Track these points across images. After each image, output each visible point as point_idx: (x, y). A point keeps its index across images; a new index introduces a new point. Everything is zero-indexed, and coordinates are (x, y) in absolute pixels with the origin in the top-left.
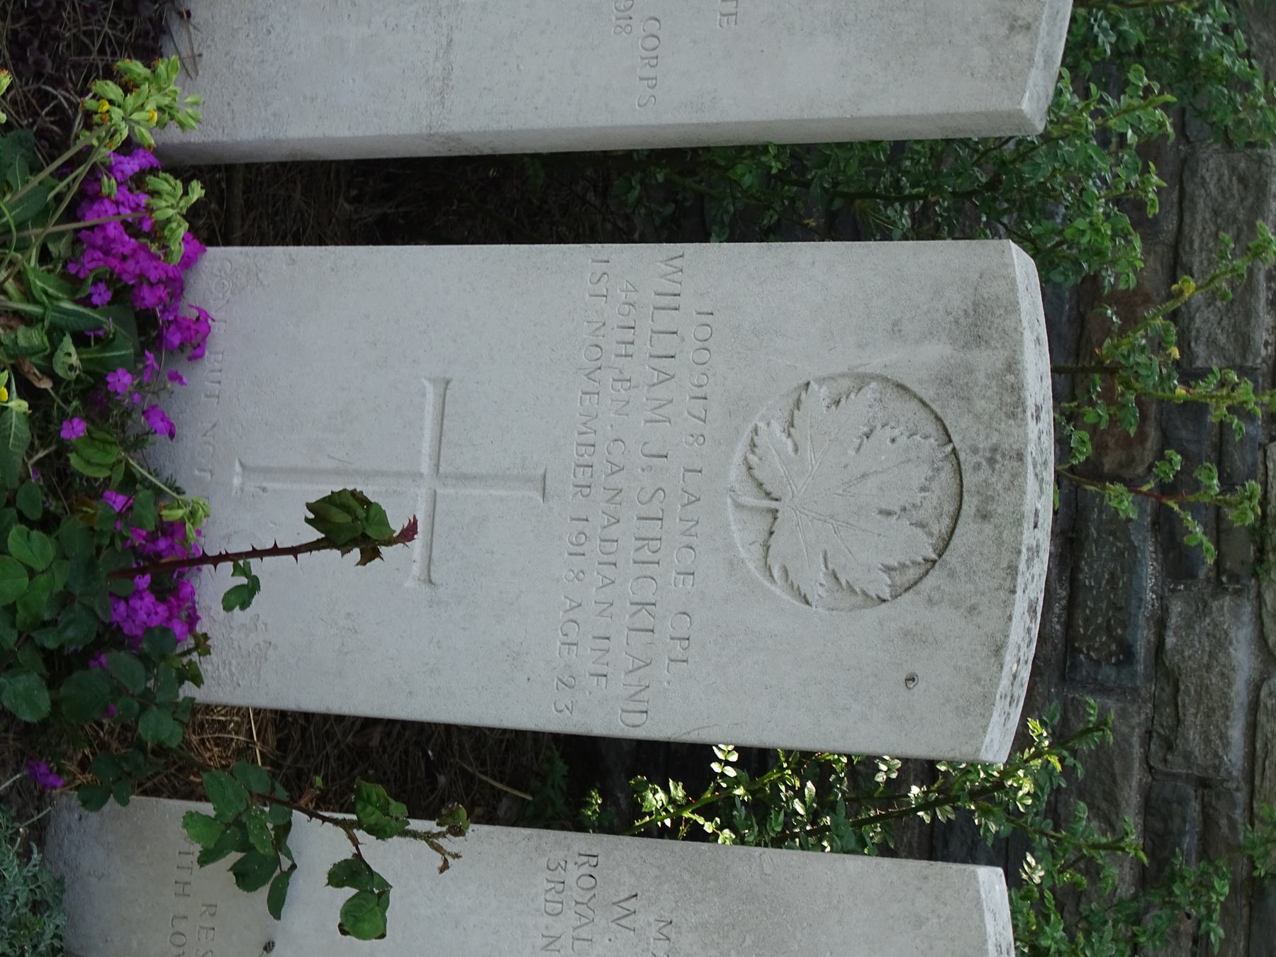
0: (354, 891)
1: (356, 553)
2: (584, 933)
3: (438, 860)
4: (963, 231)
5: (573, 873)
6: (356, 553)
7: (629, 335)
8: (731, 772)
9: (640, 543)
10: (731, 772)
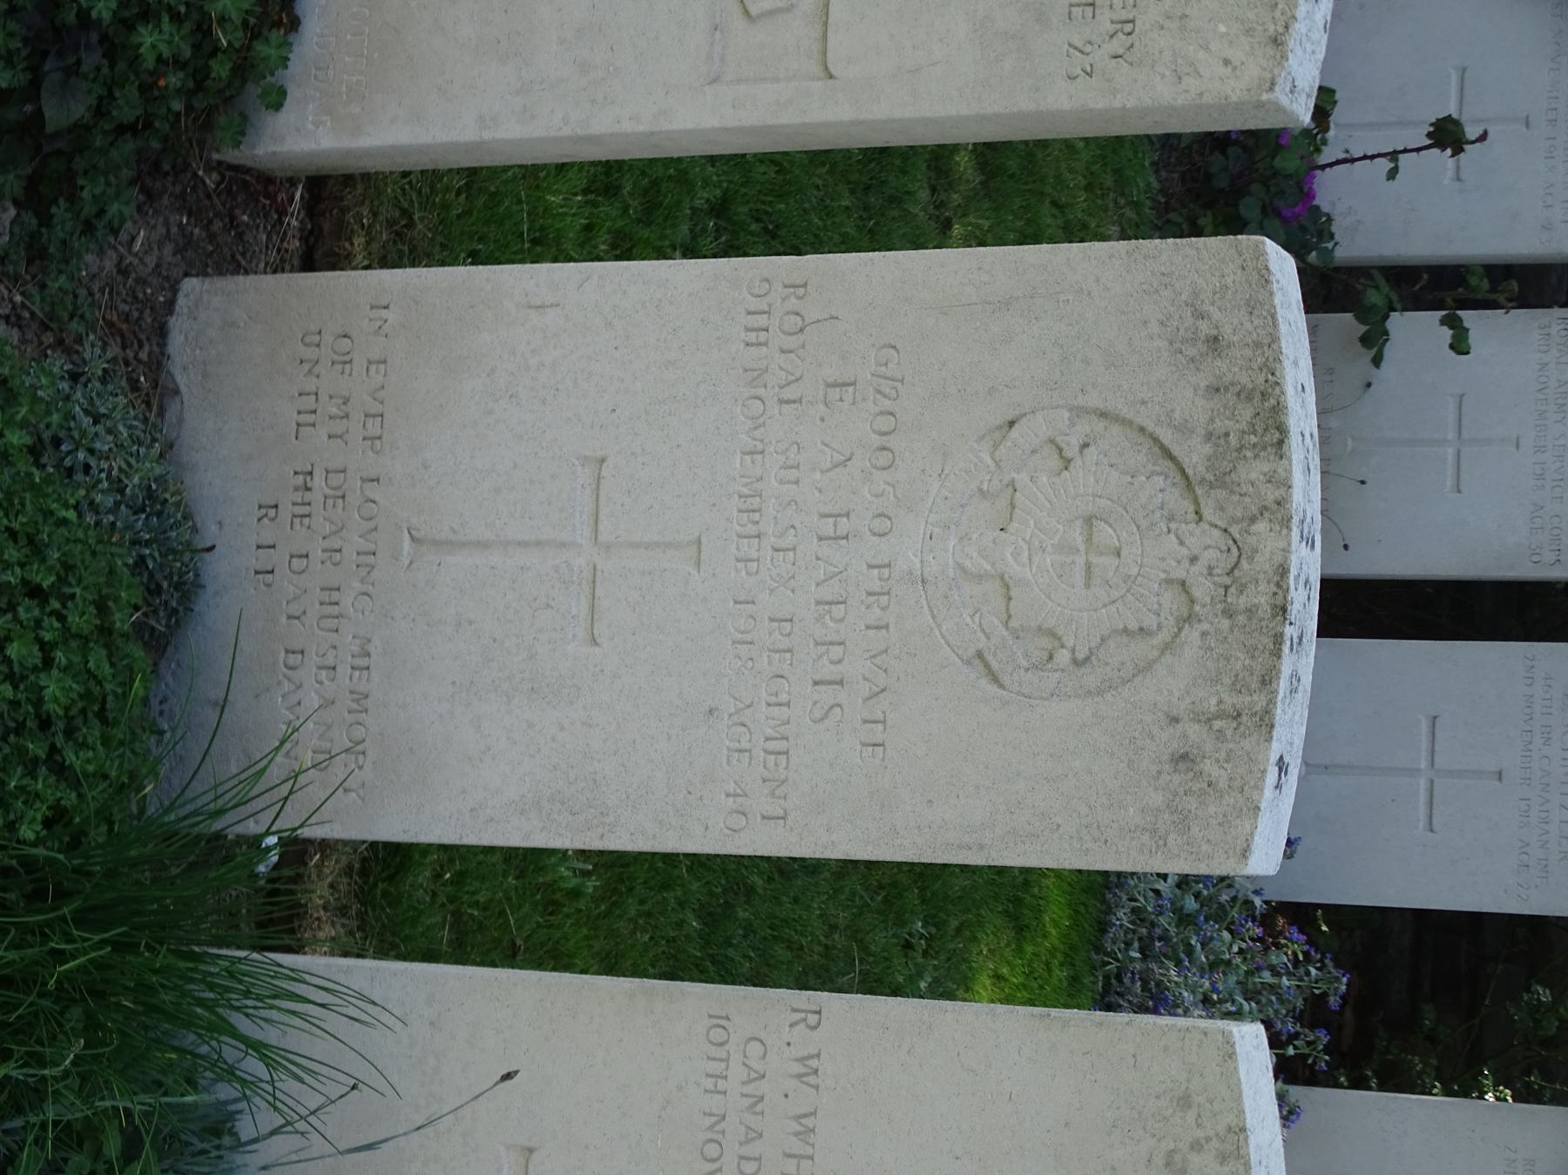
1: (1449, 152)
5: (1554, 330)
6: (1449, 152)
7: (1548, 703)
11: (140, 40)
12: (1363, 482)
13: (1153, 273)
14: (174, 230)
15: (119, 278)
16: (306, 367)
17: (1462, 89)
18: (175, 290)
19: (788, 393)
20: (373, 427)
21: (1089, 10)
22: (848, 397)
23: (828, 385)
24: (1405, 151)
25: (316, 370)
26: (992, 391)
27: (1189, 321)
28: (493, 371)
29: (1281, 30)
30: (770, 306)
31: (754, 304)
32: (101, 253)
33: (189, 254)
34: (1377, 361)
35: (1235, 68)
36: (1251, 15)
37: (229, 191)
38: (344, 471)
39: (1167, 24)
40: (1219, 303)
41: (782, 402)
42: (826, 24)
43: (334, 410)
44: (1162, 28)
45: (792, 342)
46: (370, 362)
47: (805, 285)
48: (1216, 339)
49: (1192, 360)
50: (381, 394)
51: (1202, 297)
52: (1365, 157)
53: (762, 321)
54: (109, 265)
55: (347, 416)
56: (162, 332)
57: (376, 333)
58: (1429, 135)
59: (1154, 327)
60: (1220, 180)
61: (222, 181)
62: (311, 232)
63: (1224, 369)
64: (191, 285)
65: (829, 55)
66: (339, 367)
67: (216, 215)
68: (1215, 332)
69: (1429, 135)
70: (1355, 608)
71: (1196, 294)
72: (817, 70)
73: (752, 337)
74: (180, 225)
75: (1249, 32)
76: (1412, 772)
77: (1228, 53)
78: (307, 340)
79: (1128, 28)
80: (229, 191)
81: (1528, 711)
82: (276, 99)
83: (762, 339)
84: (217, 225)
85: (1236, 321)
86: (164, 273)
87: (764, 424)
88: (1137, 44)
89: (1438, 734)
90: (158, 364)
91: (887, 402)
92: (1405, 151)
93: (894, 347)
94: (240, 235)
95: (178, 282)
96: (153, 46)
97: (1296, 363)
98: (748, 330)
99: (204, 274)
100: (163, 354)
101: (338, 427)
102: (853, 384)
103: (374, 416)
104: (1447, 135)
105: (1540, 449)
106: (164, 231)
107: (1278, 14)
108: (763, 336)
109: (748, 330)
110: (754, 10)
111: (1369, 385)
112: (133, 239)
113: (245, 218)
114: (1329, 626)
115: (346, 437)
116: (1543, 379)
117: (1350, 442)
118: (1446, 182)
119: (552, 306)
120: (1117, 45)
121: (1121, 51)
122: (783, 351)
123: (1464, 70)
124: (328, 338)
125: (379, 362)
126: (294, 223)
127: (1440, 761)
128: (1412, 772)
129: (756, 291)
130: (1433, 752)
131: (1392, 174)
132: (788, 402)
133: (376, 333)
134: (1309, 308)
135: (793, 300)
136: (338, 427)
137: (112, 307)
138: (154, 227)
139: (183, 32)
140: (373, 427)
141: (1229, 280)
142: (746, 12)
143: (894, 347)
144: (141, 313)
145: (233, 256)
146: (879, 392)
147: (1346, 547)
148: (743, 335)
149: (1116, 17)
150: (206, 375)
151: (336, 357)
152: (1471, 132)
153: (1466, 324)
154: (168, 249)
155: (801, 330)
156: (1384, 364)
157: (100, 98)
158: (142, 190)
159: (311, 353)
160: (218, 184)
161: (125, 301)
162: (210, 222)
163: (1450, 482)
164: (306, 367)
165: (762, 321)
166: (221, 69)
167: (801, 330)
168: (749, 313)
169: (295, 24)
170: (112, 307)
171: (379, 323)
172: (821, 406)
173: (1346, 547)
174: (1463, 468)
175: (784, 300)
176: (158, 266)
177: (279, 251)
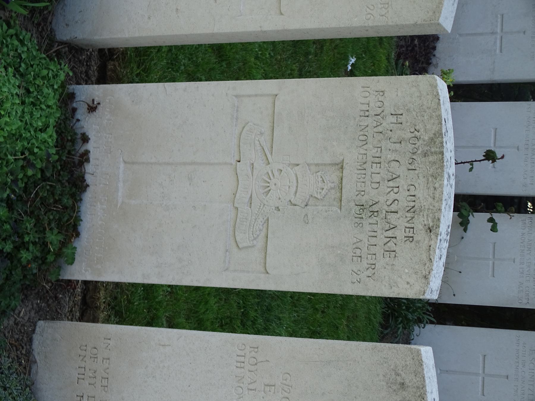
0: (449, 31)
1: (491, 161)
2: (530, 232)
3: (509, 217)
4: (243, 324)
5: (527, 221)
6: (491, 161)
7: (524, 353)
8: (531, 210)
9: (406, 239)
10: (531, 210)
11: (21, 256)
12: (460, 272)
13: (381, 357)
14: (35, 305)
15: (15, 326)
16: (81, 358)
17: (495, 135)
18: (35, 326)
19: (251, 387)
20: (105, 382)
21: (359, 258)
22: (272, 391)
23: (265, 385)
24: (476, 161)
25: (85, 359)
26: (323, 394)
27: (394, 376)
28: (147, 367)
29: (427, 274)
30: (245, 354)
31: (240, 353)
32: (9, 319)
33: (41, 313)
34: (465, 230)
35: (411, 286)
36: (417, 267)
37: (55, 288)
38: (94, 397)
39: (387, 267)
40: (404, 371)
41: (248, 389)
42: (266, 253)
43: (91, 375)
44: (385, 268)
45: (253, 368)
46: (104, 359)
47: (257, 348)
48: (403, 384)
49: (395, 390)
50: (107, 371)
51: (398, 368)
52: (462, 163)
53: (242, 359)
54: (11, 322)
55: (95, 377)
56: (31, 340)
57: (106, 348)
58: (484, 156)
59: (381, 377)
60: (414, 53)
61: (52, 285)
62: (85, 289)
63: (406, 395)
64: (41, 323)
65: (267, 265)
66: (93, 359)
67: (50, 298)
68: (402, 381)
69: (484, 156)
71: (396, 367)
72: (263, 270)
73: (239, 365)
74: (37, 304)
75: (416, 273)
76: (477, 374)
77: (408, 280)
78: (82, 348)
79: (373, 267)
80: (55, 288)
81: (517, 355)
82: (71, 261)
83: (242, 366)
84: (51, 301)
85: (410, 378)
86: (31, 321)
87: (242, 397)
88: (376, 273)
89: (486, 362)
90: (29, 353)
91: (286, 394)
92: (476, 161)
93: (289, 374)
94: (59, 303)
95: (36, 322)
96: (26, 258)
97: (432, 392)
98: (237, 362)
99: (45, 319)
100: (31, 348)
101: (92, 381)
102: (274, 386)
103: (105, 378)
104: (490, 156)
105: (522, 263)
106: (31, 307)
107: (426, 267)
108: (242, 365)
109: (237, 362)
110: (240, 246)
111: (463, 238)
112: (20, 312)
113: (61, 296)
115: (95, 385)
116: (523, 239)
118: (490, 168)
119: (168, 345)
120: (369, 272)
121: (370, 275)
122: (249, 371)
123: (496, 129)
124: (89, 348)
125: (107, 359)
126: (79, 290)
127: (486, 371)
128: (477, 374)
129: (240, 348)
130: (484, 367)
131: (471, 170)
132: (251, 390)
133: (106, 348)
135: (253, 353)
136: (92, 381)
137: (12, 337)
138: (28, 306)
139: (37, 249)
140: (105, 382)
141: (408, 363)
142: (238, 246)
143: (289, 374)
144: (23, 336)
145: (56, 310)
146: (283, 390)
147: (454, 295)
148: (235, 363)
149: (369, 262)
150: (46, 357)
151: (92, 356)
152: (499, 156)
153: (496, 221)
154: (33, 312)
155: (256, 364)
156: (467, 231)
157: (7, 275)
158: (23, 294)
159: (83, 353)
160: (51, 287)
161: (17, 334)
162: (48, 300)
163: (490, 273)
164: (81, 358)
165: (242, 359)
166: (50, 258)
167: (256, 364)
168: (238, 356)
169: (78, 235)
170: (12, 337)
171: (107, 345)
172: (263, 392)
173: (454, 295)
175: (250, 352)
176: (29, 318)
177: (73, 302)
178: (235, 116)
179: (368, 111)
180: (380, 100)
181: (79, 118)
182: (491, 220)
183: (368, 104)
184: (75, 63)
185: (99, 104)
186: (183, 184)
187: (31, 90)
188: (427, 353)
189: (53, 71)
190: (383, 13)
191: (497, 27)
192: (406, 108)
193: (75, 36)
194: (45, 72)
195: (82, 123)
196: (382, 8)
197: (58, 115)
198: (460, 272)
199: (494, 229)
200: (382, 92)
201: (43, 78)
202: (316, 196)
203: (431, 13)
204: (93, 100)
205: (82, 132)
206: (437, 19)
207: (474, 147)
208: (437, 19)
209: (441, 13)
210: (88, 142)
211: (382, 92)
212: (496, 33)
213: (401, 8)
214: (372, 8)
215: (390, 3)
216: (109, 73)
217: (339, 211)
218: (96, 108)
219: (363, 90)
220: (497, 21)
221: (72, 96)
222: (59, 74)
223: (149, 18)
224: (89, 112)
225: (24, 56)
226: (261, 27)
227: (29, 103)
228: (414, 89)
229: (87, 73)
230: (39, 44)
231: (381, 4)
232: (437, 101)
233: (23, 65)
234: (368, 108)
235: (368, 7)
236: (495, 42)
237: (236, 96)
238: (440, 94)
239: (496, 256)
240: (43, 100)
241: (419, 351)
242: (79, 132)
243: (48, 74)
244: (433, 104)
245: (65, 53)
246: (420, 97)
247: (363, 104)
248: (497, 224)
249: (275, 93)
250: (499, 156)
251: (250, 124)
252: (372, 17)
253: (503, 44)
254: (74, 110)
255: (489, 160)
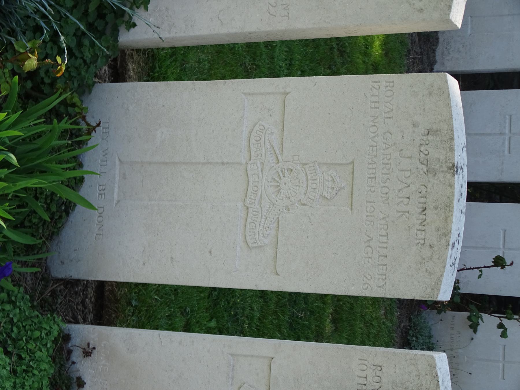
0: (459, 26)
1: (500, 267)
6: (500, 267)
12: (470, 374)
17: (510, 148)
24: (485, 267)
34: (475, 331)
52: (471, 269)
58: (493, 262)
69: (493, 262)
70: (478, 192)
92: (485, 267)
104: (499, 262)
111: (472, 339)
114: (471, 198)
117: (466, 358)
123: (505, 230)
131: (480, 276)
134: (461, 90)
156: (477, 333)
163: (501, 376)
174: (505, 371)
178: (231, 376)
179: (365, 385)
180: (377, 375)
181: (75, 361)
182: (501, 326)
183: (366, 378)
184: (71, 296)
185: (94, 348)
186: (195, 183)
187: (23, 356)
188: (441, 359)
189: (45, 329)
190: (381, 285)
191: (505, 127)
192: (404, 386)
193: (70, 275)
194: (37, 334)
195: (77, 366)
196: (379, 279)
197: (52, 372)
198: (470, 374)
199: (504, 335)
200: (380, 366)
201: (36, 340)
202: (326, 196)
203: (429, 290)
204: (89, 344)
205: (78, 376)
206: (435, 296)
207: (484, 248)
208: (435, 296)
209: (440, 290)
210: (83, 387)
211: (380, 366)
212: (504, 134)
213: (399, 281)
214: (369, 277)
215: (387, 275)
216: (107, 294)
217: (350, 212)
218: (91, 353)
219: (360, 362)
220: (505, 122)
221: (67, 338)
222: (52, 330)
223: (144, 264)
224: (84, 357)
225: (15, 320)
226: (256, 286)
227: (20, 372)
228: (413, 367)
229: (83, 302)
230: (32, 300)
231: (384, 154)
232: (436, 382)
233: (15, 329)
234: (365, 382)
235: (365, 276)
236: (504, 143)
237: (232, 355)
238: (439, 375)
239: (506, 359)
240: (35, 366)
241: (432, 357)
242: (74, 376)
243: (41, 335)
244: (432, 385)
245: (60, 291)
246: (418, 376)
247: (360, 377)
248: (507, 329)
249: (272, 356)
250: (508, 263)
251: (245, 385)
252: (369, 287)
253: (511, 144)
254: (70, 352)
255: (498, 266)
